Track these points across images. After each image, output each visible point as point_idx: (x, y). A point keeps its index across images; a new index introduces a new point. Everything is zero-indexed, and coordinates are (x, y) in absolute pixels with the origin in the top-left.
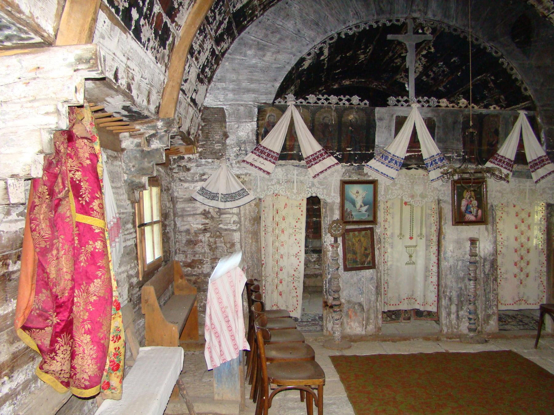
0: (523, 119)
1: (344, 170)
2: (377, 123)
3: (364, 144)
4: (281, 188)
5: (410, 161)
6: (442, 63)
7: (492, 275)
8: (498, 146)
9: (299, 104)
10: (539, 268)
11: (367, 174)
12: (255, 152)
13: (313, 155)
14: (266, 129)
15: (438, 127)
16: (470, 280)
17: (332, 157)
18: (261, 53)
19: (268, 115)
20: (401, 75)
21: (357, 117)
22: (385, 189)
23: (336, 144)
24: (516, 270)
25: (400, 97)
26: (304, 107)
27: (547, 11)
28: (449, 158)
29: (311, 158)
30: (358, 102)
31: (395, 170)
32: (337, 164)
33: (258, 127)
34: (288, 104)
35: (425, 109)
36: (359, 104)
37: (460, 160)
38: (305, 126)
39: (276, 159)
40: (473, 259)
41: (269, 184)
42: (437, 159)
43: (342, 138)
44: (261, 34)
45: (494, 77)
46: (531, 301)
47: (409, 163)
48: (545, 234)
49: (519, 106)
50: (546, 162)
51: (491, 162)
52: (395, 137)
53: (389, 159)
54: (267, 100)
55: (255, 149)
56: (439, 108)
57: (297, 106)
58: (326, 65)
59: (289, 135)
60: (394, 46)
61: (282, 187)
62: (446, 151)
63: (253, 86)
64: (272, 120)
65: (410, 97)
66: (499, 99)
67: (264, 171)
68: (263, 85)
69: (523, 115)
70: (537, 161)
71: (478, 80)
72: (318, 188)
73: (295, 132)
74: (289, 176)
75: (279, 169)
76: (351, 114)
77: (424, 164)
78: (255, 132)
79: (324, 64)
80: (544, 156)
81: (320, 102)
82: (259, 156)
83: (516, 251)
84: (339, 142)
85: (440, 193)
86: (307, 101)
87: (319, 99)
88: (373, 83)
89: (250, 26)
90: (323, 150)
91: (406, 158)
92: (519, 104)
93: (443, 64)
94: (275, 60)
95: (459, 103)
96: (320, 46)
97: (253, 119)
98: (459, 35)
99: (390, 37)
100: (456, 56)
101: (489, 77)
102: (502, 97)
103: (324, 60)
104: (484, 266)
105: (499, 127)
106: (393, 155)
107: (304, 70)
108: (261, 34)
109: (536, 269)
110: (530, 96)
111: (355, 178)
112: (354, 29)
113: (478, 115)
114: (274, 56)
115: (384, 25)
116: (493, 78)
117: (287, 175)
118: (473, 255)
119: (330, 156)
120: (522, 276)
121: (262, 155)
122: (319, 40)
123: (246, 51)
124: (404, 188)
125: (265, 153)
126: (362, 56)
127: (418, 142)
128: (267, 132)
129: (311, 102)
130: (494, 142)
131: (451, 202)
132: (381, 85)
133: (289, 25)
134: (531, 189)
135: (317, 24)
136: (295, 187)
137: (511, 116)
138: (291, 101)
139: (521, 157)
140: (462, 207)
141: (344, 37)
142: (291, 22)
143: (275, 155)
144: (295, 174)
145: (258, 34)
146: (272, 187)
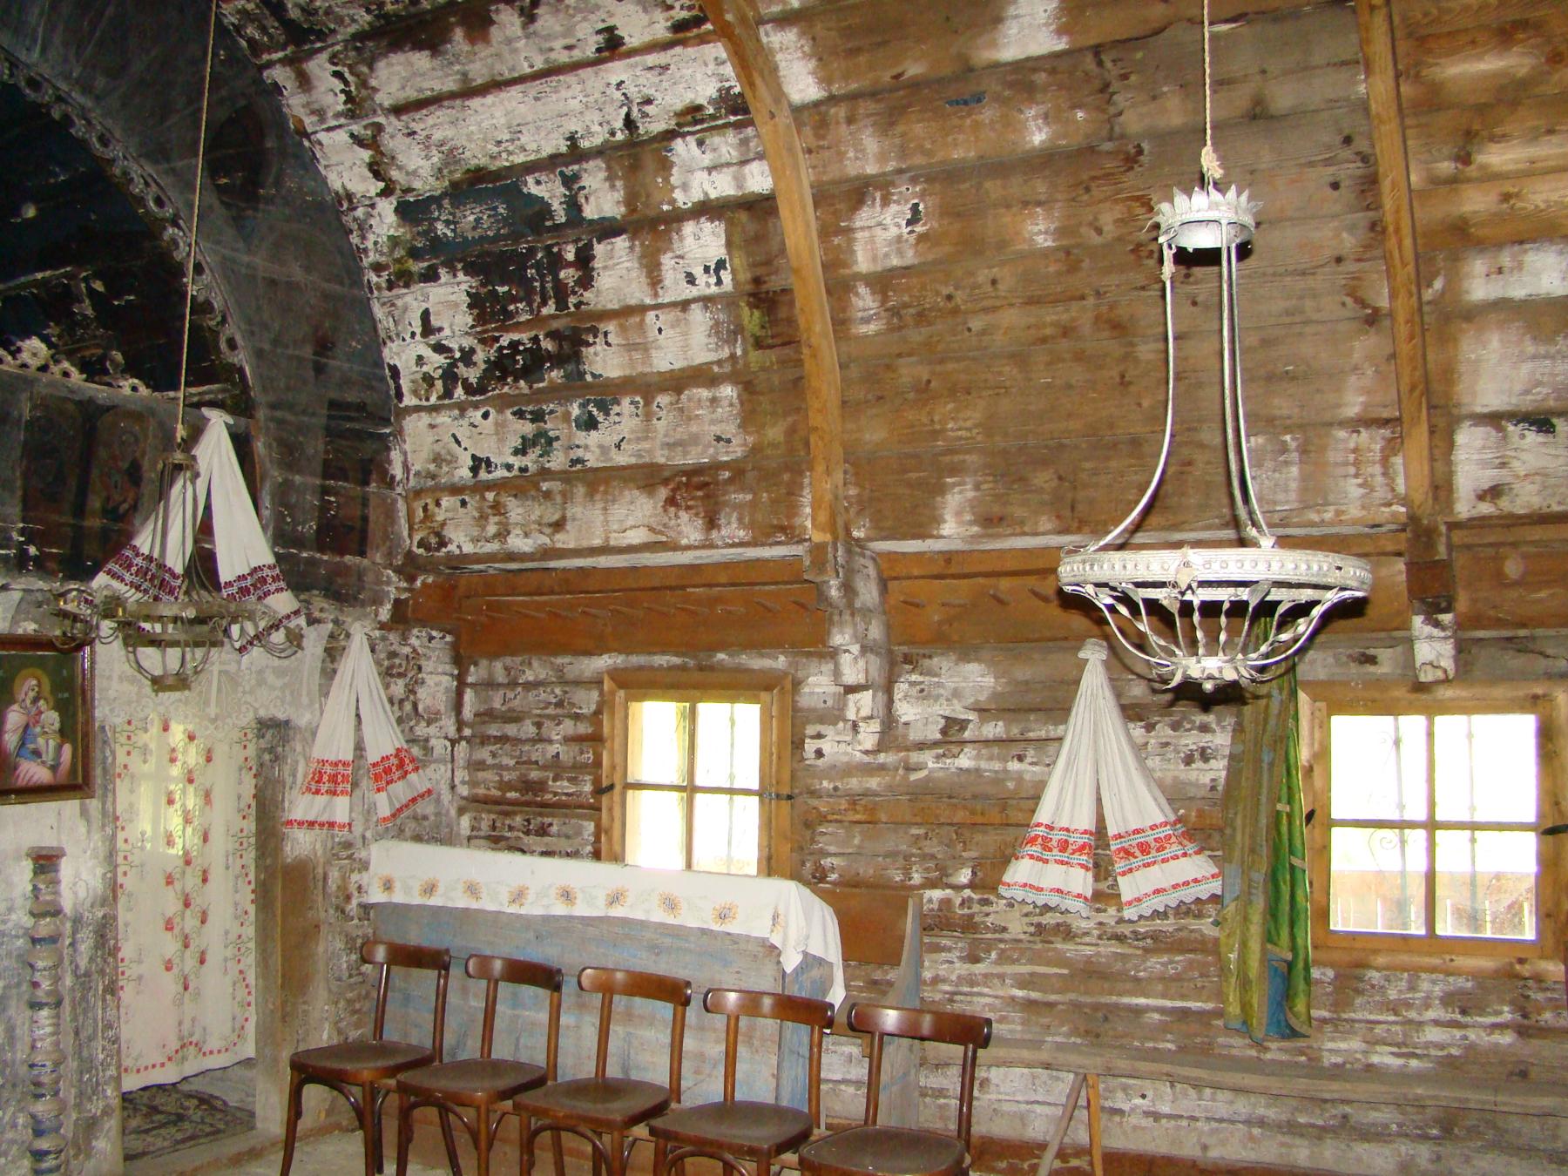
7: (102, 972)
8: (137, 522)
10: (236, 930)
16: (35, 1005)
24: (171, 946)
27: (315, 118)
40: (45, 927)
45: (105, 286)
46: (213, 1043)
48: (252, 818)
50: (273, 588)
51: (114, 576)
66: (102, 359)
69: (218, 424)
70: (249, 581)
71: (36, 283)
83: (170, 881)
95: (19, 350)
101: (86, 280)
102: (118, 356)
104: (72, 944)
105: (144, 454)
109: (227, 933)
110: (241, 371)
113: (80, 402)
116: (98, 286)
118: (47, 910)
120: (190, 962)
130: (126, 506)
134: (226, 672)
139: (203, 565)
140: (7, 737)
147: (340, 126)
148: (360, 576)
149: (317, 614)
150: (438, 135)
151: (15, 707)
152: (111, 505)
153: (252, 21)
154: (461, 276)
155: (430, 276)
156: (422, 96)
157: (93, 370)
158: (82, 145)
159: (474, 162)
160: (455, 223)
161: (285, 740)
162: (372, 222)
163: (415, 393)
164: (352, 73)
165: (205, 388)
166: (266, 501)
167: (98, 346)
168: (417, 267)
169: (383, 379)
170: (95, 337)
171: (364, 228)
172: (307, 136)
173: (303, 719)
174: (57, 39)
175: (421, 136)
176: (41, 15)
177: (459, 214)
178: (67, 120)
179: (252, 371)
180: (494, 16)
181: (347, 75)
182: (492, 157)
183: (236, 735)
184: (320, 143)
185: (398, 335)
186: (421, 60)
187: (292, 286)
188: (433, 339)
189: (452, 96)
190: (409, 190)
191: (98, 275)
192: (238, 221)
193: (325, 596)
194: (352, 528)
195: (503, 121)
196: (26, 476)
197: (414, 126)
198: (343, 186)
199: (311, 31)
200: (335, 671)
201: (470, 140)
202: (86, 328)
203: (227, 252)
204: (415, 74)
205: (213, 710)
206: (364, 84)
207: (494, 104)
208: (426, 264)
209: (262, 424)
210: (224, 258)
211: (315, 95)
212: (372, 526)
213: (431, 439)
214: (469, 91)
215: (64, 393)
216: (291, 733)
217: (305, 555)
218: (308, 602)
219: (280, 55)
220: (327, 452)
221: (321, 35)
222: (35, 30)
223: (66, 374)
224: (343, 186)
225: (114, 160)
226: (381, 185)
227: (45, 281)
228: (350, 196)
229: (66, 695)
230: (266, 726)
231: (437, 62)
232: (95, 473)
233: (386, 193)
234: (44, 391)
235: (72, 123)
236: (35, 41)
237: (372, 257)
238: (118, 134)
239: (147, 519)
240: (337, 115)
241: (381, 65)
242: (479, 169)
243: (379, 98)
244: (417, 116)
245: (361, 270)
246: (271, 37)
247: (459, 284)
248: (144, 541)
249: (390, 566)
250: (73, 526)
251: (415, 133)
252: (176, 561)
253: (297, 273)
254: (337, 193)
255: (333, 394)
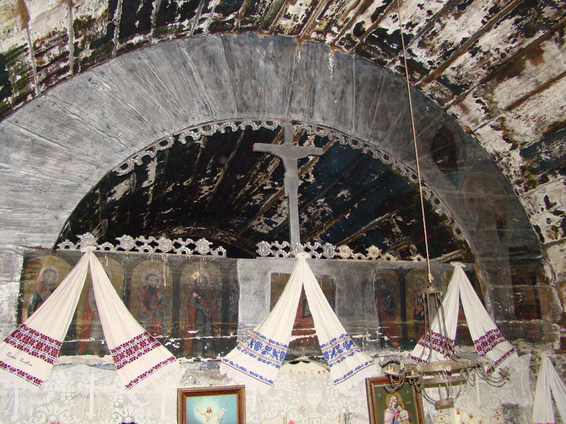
0: (460, 275)
1: (184, 371)
2: (241, 286)
3: (220, 323)
4: (62, 409)
5: (298, 350)
6: (323, 200)
9: (102, 250)
11: (225, 376)
12: (13, 339)
13: (127, 344)
14: (38, 296)
15: (340, 291)
17: (162, 347)
18: (37, 158)
19: (42, 270)
20: (259, 220)
21: (207, 276)
22: (257, 401)
23: (170, 323)
25: (277, 242)
26: (112, 255)
27: (474, 124)
28: (359, 342)
29: (123, 349)
30: (208, 249)
31: (274, 367)
32: (171, 359)
33: (21, 291)
34: (82, 250)
35: (318, 260)
36: (209, 253)
37: (375, 343)
38: (114, 291)
39: (54, 353)
41: (39, 403)
42: (341, 344)
43: (181, 312)
44: (39, 125)
45: (402, 218)
47: (295, 352)
49: (441, 258)
50: (498, 340)
52: (271, 310)
53: (263, 348)
54: (43, 242)
55: (13, 335)
56: (338, 260)
57: (98, 254)
58: (150, 199)
59: (82, 308)
60: (255, 172)
61: (65, 408)
62: (354, 330)
63: (18, 216)
64: (50, 279)
65: (292, 242)
66: (408, 249)
67: (29, 378)
68: (37, 215)
69: (459, 268)
70: (486, 339)
72: (137, 406)
73: (95, 302)
74: (79, 385)
75: (61, 373)
76: (196, 270)
77: (321, 354)
78: (14, 301)
79: (147, 196)
80: (495, 331)
81: (141, 249)
82: (20, 347)
84: (175, 319)
85: (349, 402)
86: (118, 246)
87: (140, 244)
88: (217, 232)
89: (20, 111)
90: (146, 334)
91: (294, 345)
92: (440, 256)
93: (324, 202)
94: (63, 172)
95: (367, 252)
96: (144, 154)
97: (12, 276)
98: (361, 150)
99: (258, 147)
100: (345, 189)
101: (394, 217)
102: (414, 247)
103: (147, 188)
106: (270, 340)
107: (114, 202)
108: (39, 125)
110: (465, 242)
111: (204, 384)
112: (201, 131)
113: (397, 270)
114: (62, 165)
115: (249, 128)
116: (400, 219)
117: (75, 385)
119: (158, 345)
121: (27, 346)
122: (142, 145)
123: (8, 153)
124: (290, 398)
125: (32, 343)
126: (206, 188)
127: (310, 316)
128: (39, 302)
129: (125, 248)
131: (367, 416)
132: (228, 236)
133: (92, 116)
135: (140, 119)
136: (91, 408)
137: (442, 272)
138: (89, 245)
141: (184, 142)
142: (96, 111)
143: (53, 345)
144: (92, 382)
145: (35, 125)
146: (44, 409)
147: (485, 124)
148: (541, 328)
149: (522, 350)
150: (531, 114)
151: (388, 410)
152: (417, 313)
153: (437, 91)
154: (559, 176)
155: (544, 180)
156: (518, 98)
157: (405, 255)
158: (378, 161)
159: (552, 120)
160: (550, 152)
161: (518, 415)
162: (511, 162)
163: (550, 236)
164: (484, 99)
165: (452, 253)
166: (488, 300)
167: (405, 244)
168: (537, 177)
169: (533, 233)
170: (403, 240)
171: (508, 166)
172: (472, 133)
173: (524, 403)
174: (360, 121)
175: (523, 116)
176: (352, 115)
177: (551, 148)
178: (371, 153)
179: (470, 241)
180: (543, 48)
181: (482, 100)
182: (561, 116)
183: (493, 413)
184: (479, 134)
185: (535, 211)
186: (514, 82)
187: (480, 200)
188: (552, 209)
189: (533, 93)
190: (525, 143)
191: (398, 215)
192: (450, 177)
193: (524, 341)
194: (532, 306)
195: (561, 96)
196: (378, 305)
197: (519, 113)
198: (494, 150)
199: (462, 86)
200: (536, 377)
201: (547, 111)
202: (399, 237)
203: (448, 191)
204: (513, 89)
205: (479, 403)
206: (491, 102)
207: (554, 91)
208: (540, 175)
209: (479, 264)
210: (447, 194)
211: (471, 114)
212: (542, 304)
213: (562, 257)
214: (541, 88)
215: (389, 267)
216: (520, 410)
217: (511, 322)
218: (516, 345)
219: (452, 101)
220: (512, 272)
221: (466, 87)
222: (351, 122)
223: (388, 259)
224: (494, 150)
225: (392, 165)
226: (511, 145)
227: (379, 222)
228: (498, 154)
229: (410, 402)
230: (507, 407)
231: (521, 80)
232: (408, 300)
233: (514, 148)
234: (380, 268)
235: (372, 154)
236: (352, 125)
237: (515, 179)
238: (391, 153)
239: (434, 317)
240: (483, 119)
241: (496, 90)
242: (555, 123)
243: (499, 106)
244: (519, 108)
245: (511, 186)
246: (446, 95)
247: (559, 180)
248: (435, 327)
249: (555, 321)
250: (402, 325)
251: (520, 116)
252: (452, 335)
253: (481, 193)
254: (492, 154)
255: (511, 245)
